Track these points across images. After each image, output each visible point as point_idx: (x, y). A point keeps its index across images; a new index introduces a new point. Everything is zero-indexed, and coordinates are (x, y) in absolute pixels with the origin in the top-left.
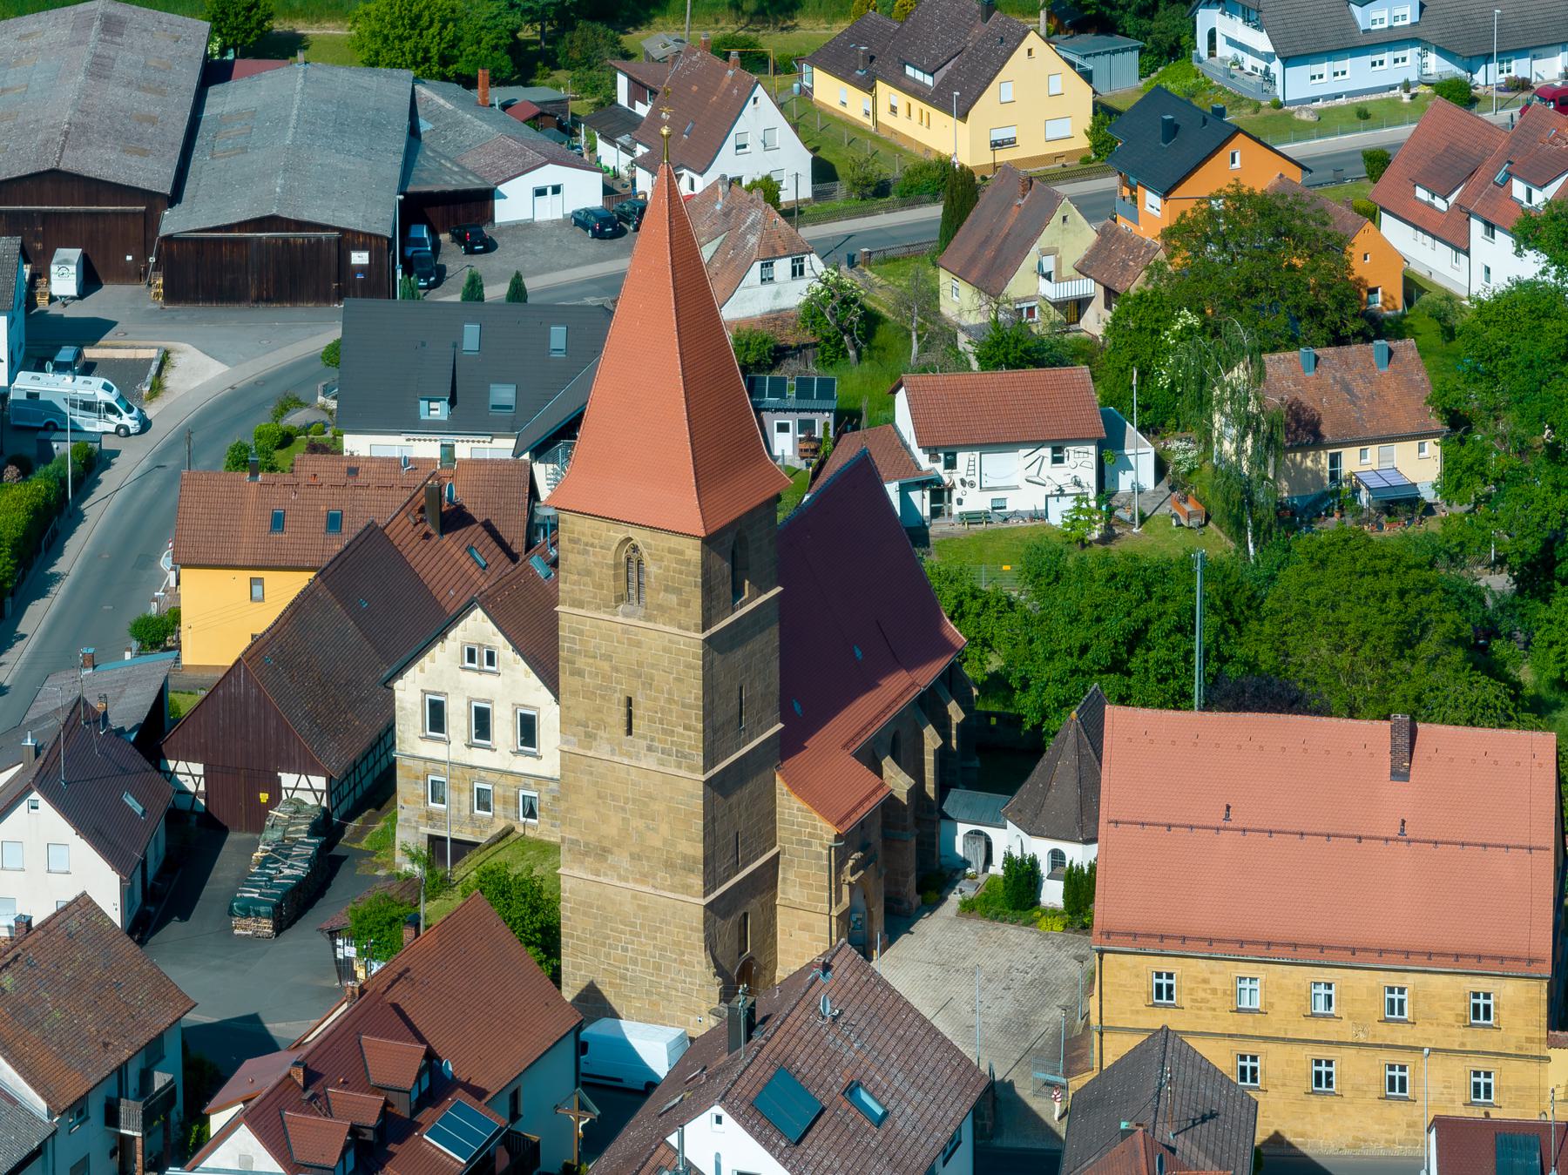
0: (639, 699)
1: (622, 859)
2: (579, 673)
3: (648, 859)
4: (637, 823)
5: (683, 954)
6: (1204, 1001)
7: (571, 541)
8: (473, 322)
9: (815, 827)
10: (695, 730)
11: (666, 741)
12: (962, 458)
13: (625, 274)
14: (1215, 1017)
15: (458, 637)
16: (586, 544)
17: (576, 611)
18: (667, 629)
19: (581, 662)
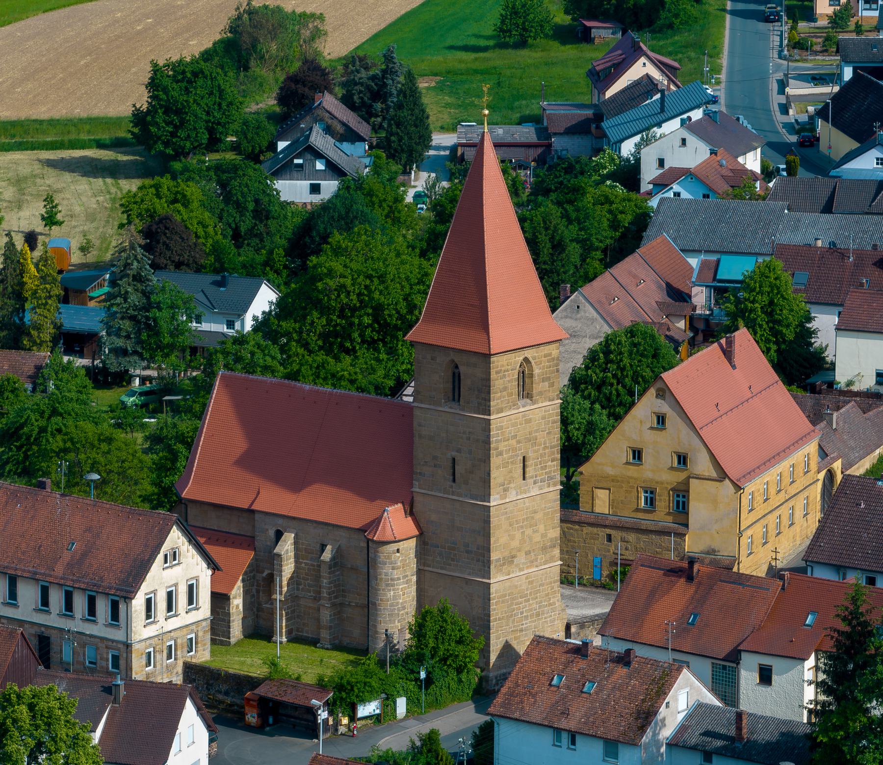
0: (531, 455)
1: (521, 559)
5: (550, 599)
8: (276, 287)
13: (875, 264)
17: (500, 415)
18: (544, 404)
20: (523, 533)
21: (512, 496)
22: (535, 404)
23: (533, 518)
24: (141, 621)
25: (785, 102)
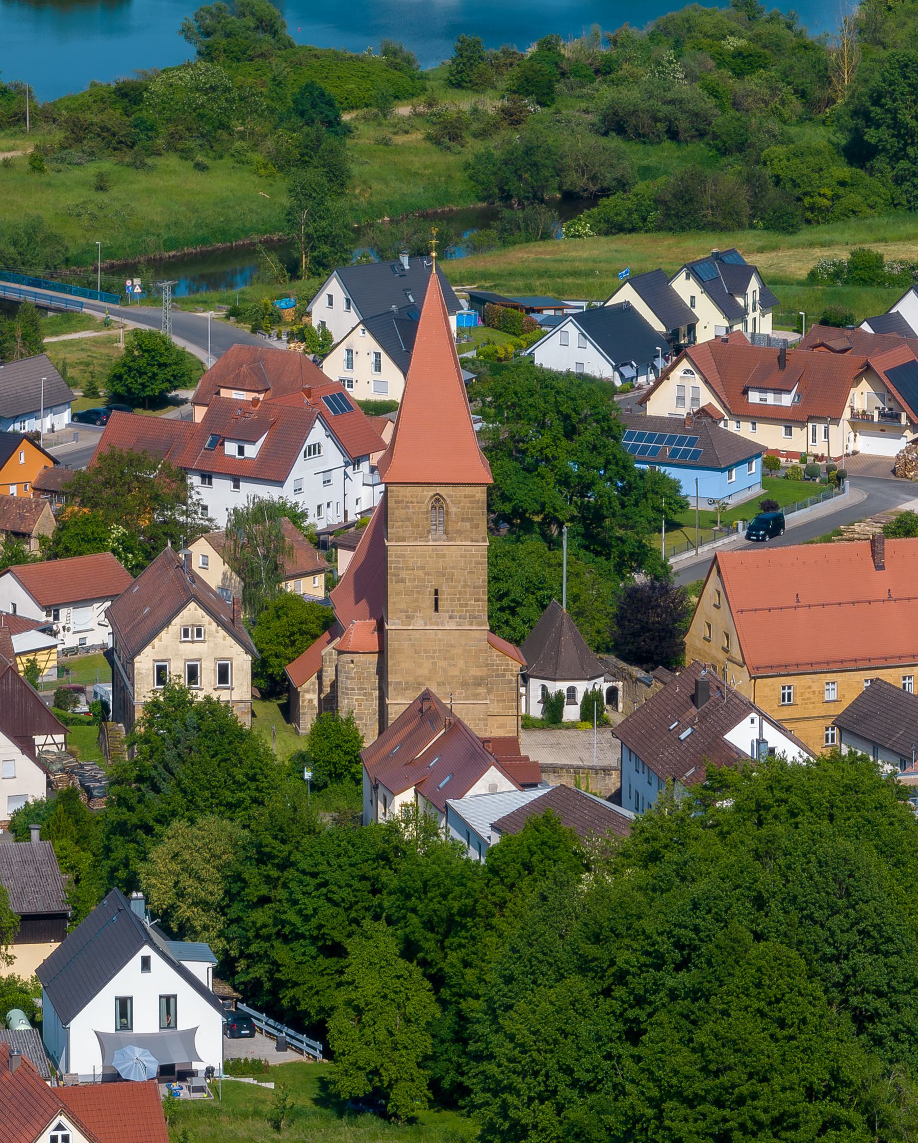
2: (403, 581)
3: (450, 684)
4: (442, 663)
6: (809, 699)
7: (396, 502)
9: (507, 665)
10: (482, 600)
11: (462, 611)
12: (63, 612)
14: (814, 708)
15: (178, 623)
16: (408, 502)
19: (403, 574)
20: (434, 663)
21: (418, 624)
22: (451, 540)
23: (449, 651)
24: (148, 684)
25: (628, 284)
